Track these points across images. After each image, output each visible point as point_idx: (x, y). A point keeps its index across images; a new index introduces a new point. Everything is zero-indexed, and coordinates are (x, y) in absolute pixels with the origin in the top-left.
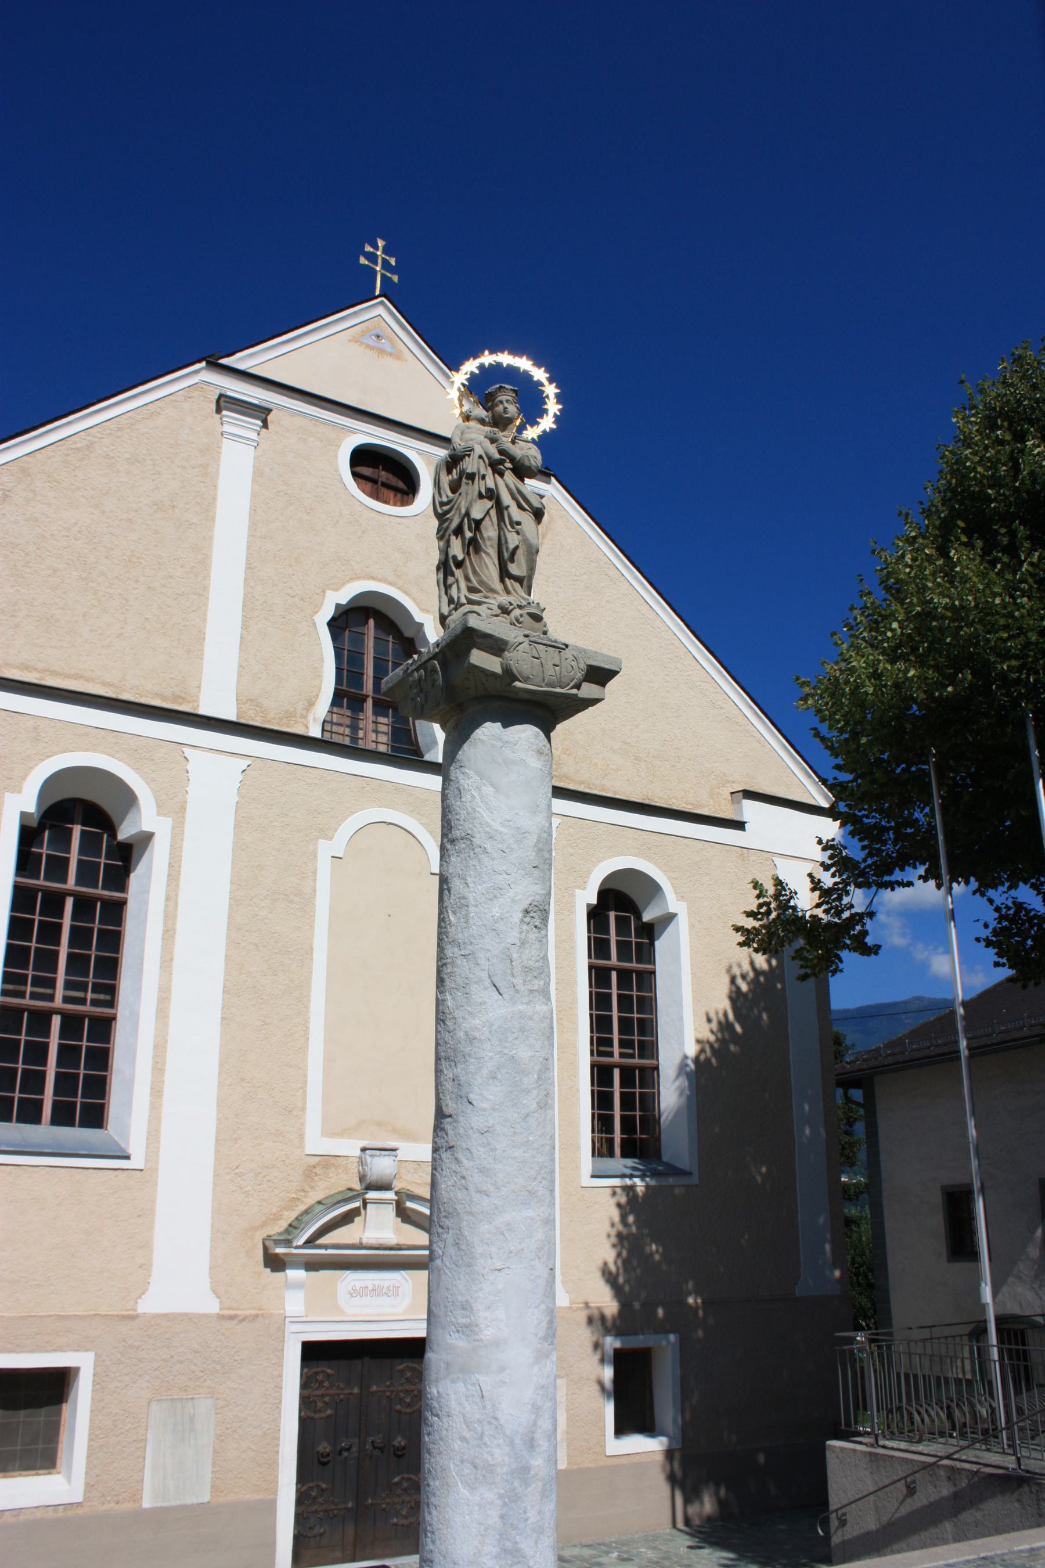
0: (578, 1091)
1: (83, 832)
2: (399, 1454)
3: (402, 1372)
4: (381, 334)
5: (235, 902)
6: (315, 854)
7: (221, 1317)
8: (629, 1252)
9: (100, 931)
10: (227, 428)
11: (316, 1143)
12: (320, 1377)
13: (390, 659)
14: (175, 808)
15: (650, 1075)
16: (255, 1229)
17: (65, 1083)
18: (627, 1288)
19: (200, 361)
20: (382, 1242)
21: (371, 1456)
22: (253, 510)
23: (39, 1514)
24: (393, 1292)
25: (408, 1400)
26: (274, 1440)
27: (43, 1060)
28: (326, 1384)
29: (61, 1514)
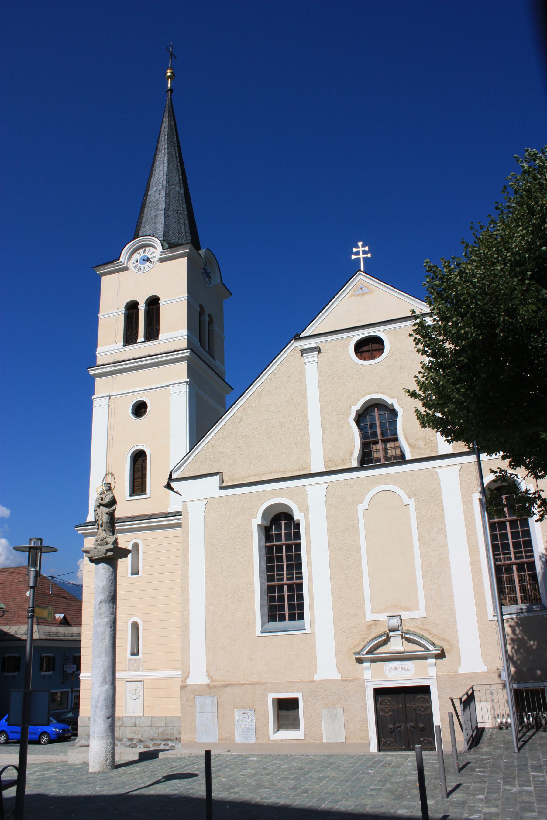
0: (483, 580)
1: (285, 523)
2: (422, 730)
3: (419, 699)
4: (362, 286)
5: (330, 536)
6: (357, 511)
7: (342, 680)
8: (518, 646)
9: (295, 555)
10: (306, 361)
11: (370, 617)
12: (386, 701)
13: (387, 420)
14: (305, 509)
15: (532, 566)
16: (351, 649)
17: (291, 607)
18: (519, 662)
19: (292, 340)
20: (398, 650)
21: (410, 730)
22: (320, 387)
23: (292, 742)
24: (408, 669)
25: (423, 709)
26: (365, 721)
27: (283, 601)
28: (388, 703)
29: (299, 742)
